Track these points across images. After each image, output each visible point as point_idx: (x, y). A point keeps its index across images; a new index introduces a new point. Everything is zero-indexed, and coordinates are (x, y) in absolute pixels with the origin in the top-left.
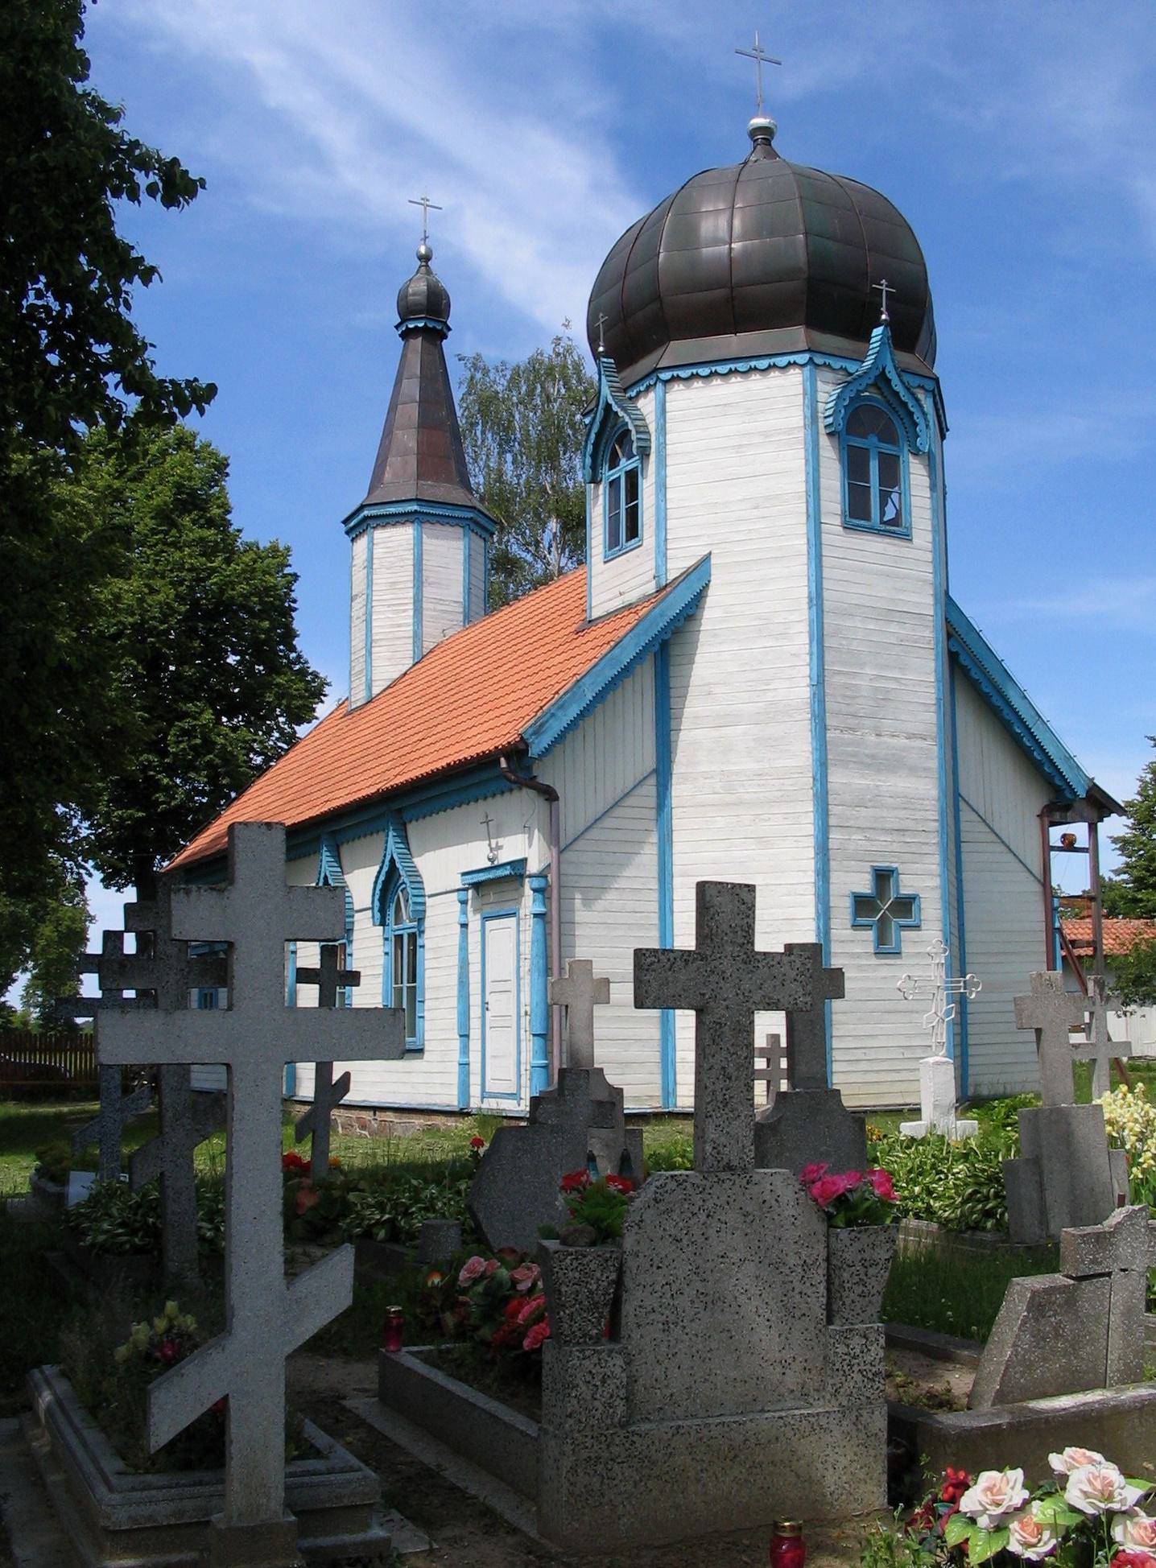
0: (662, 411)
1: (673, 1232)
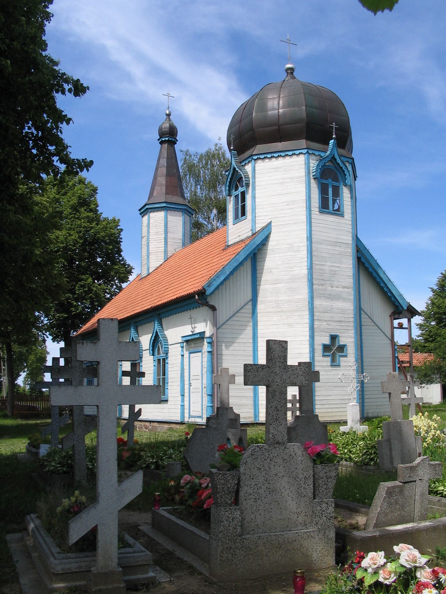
0: (254, 170)
1: (258, 466)
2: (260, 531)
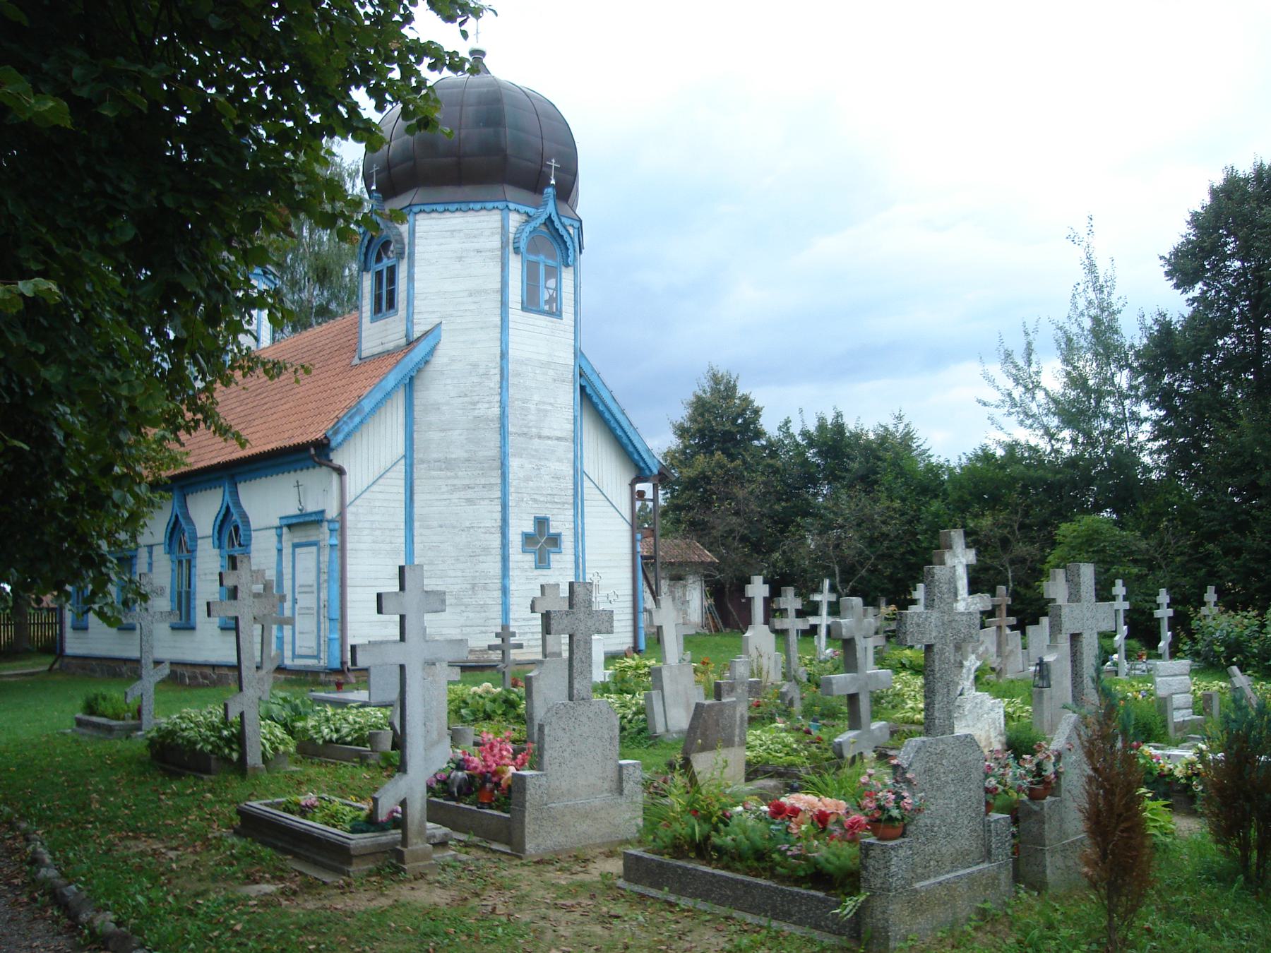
0: (412, 233)
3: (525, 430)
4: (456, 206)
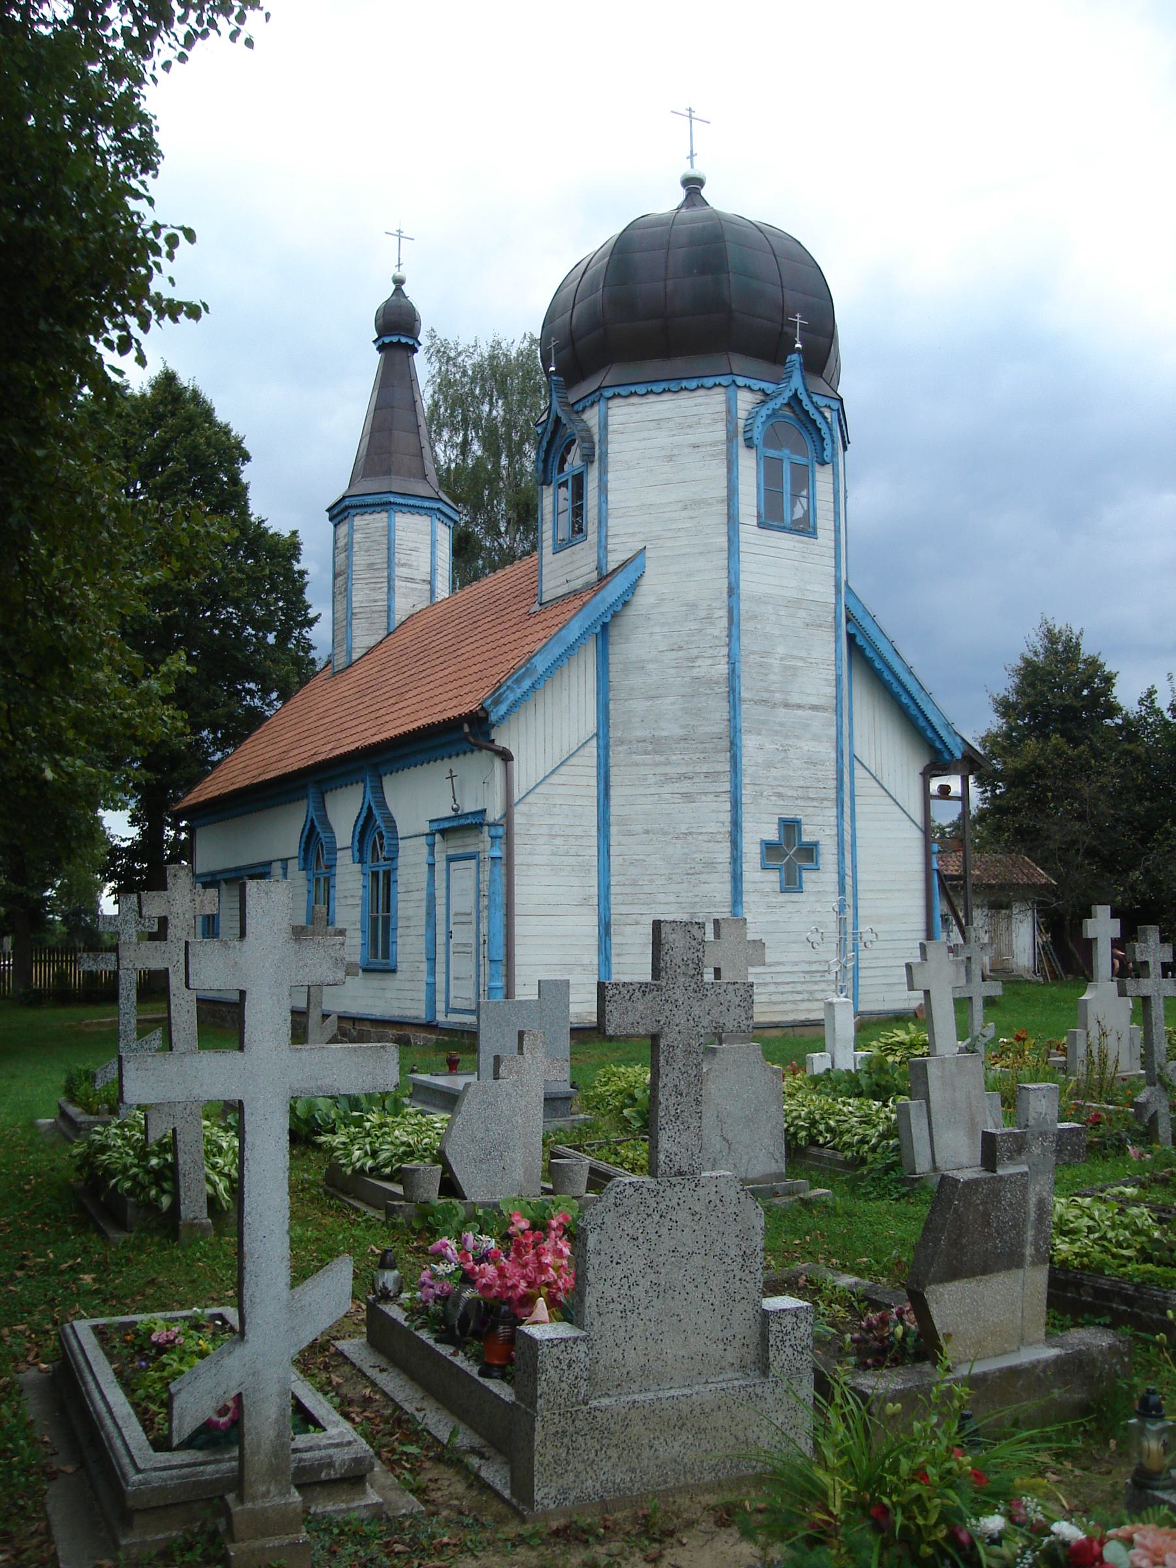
0: (604, 426)
1: (631, 1232)
2: (635, 1387)
3: (765, 695)
4: (664, 385)
